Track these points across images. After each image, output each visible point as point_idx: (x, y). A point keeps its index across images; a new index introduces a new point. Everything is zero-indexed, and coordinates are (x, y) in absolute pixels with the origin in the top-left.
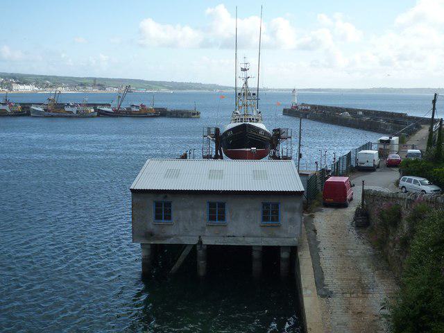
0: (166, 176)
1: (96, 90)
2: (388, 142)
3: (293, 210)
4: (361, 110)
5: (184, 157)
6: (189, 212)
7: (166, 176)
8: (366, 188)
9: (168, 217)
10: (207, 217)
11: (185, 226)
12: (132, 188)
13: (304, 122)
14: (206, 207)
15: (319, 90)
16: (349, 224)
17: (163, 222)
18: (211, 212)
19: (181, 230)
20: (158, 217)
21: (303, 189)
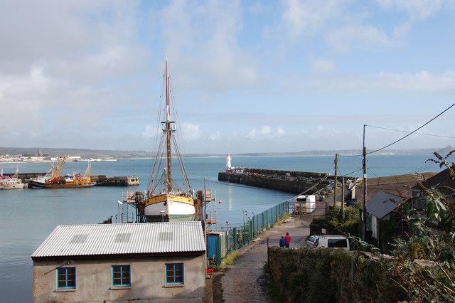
0: (73, 241)
1: (41, 159)
2: (304, 200)
3: (196, 270)
4: (289, 172)
5: (109, 222)
6: (93, 276)
7: (73, 241)
8: (270, 246)
9: (73, 284)
10: (112, 281)
11: (89, 292)
12: (33, 255)
13: (331, 174)
14: (112, 269)
15: (256, 154)
16: (254, 281)
17: (67, 288)
18: (115, 275)
19: (85, 296)
20: (61, 284)
21: (205, 249)
